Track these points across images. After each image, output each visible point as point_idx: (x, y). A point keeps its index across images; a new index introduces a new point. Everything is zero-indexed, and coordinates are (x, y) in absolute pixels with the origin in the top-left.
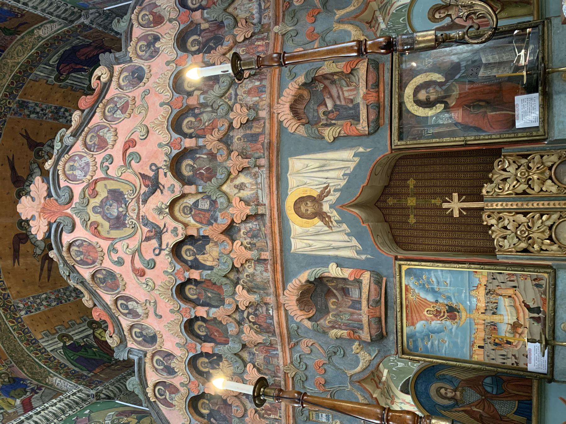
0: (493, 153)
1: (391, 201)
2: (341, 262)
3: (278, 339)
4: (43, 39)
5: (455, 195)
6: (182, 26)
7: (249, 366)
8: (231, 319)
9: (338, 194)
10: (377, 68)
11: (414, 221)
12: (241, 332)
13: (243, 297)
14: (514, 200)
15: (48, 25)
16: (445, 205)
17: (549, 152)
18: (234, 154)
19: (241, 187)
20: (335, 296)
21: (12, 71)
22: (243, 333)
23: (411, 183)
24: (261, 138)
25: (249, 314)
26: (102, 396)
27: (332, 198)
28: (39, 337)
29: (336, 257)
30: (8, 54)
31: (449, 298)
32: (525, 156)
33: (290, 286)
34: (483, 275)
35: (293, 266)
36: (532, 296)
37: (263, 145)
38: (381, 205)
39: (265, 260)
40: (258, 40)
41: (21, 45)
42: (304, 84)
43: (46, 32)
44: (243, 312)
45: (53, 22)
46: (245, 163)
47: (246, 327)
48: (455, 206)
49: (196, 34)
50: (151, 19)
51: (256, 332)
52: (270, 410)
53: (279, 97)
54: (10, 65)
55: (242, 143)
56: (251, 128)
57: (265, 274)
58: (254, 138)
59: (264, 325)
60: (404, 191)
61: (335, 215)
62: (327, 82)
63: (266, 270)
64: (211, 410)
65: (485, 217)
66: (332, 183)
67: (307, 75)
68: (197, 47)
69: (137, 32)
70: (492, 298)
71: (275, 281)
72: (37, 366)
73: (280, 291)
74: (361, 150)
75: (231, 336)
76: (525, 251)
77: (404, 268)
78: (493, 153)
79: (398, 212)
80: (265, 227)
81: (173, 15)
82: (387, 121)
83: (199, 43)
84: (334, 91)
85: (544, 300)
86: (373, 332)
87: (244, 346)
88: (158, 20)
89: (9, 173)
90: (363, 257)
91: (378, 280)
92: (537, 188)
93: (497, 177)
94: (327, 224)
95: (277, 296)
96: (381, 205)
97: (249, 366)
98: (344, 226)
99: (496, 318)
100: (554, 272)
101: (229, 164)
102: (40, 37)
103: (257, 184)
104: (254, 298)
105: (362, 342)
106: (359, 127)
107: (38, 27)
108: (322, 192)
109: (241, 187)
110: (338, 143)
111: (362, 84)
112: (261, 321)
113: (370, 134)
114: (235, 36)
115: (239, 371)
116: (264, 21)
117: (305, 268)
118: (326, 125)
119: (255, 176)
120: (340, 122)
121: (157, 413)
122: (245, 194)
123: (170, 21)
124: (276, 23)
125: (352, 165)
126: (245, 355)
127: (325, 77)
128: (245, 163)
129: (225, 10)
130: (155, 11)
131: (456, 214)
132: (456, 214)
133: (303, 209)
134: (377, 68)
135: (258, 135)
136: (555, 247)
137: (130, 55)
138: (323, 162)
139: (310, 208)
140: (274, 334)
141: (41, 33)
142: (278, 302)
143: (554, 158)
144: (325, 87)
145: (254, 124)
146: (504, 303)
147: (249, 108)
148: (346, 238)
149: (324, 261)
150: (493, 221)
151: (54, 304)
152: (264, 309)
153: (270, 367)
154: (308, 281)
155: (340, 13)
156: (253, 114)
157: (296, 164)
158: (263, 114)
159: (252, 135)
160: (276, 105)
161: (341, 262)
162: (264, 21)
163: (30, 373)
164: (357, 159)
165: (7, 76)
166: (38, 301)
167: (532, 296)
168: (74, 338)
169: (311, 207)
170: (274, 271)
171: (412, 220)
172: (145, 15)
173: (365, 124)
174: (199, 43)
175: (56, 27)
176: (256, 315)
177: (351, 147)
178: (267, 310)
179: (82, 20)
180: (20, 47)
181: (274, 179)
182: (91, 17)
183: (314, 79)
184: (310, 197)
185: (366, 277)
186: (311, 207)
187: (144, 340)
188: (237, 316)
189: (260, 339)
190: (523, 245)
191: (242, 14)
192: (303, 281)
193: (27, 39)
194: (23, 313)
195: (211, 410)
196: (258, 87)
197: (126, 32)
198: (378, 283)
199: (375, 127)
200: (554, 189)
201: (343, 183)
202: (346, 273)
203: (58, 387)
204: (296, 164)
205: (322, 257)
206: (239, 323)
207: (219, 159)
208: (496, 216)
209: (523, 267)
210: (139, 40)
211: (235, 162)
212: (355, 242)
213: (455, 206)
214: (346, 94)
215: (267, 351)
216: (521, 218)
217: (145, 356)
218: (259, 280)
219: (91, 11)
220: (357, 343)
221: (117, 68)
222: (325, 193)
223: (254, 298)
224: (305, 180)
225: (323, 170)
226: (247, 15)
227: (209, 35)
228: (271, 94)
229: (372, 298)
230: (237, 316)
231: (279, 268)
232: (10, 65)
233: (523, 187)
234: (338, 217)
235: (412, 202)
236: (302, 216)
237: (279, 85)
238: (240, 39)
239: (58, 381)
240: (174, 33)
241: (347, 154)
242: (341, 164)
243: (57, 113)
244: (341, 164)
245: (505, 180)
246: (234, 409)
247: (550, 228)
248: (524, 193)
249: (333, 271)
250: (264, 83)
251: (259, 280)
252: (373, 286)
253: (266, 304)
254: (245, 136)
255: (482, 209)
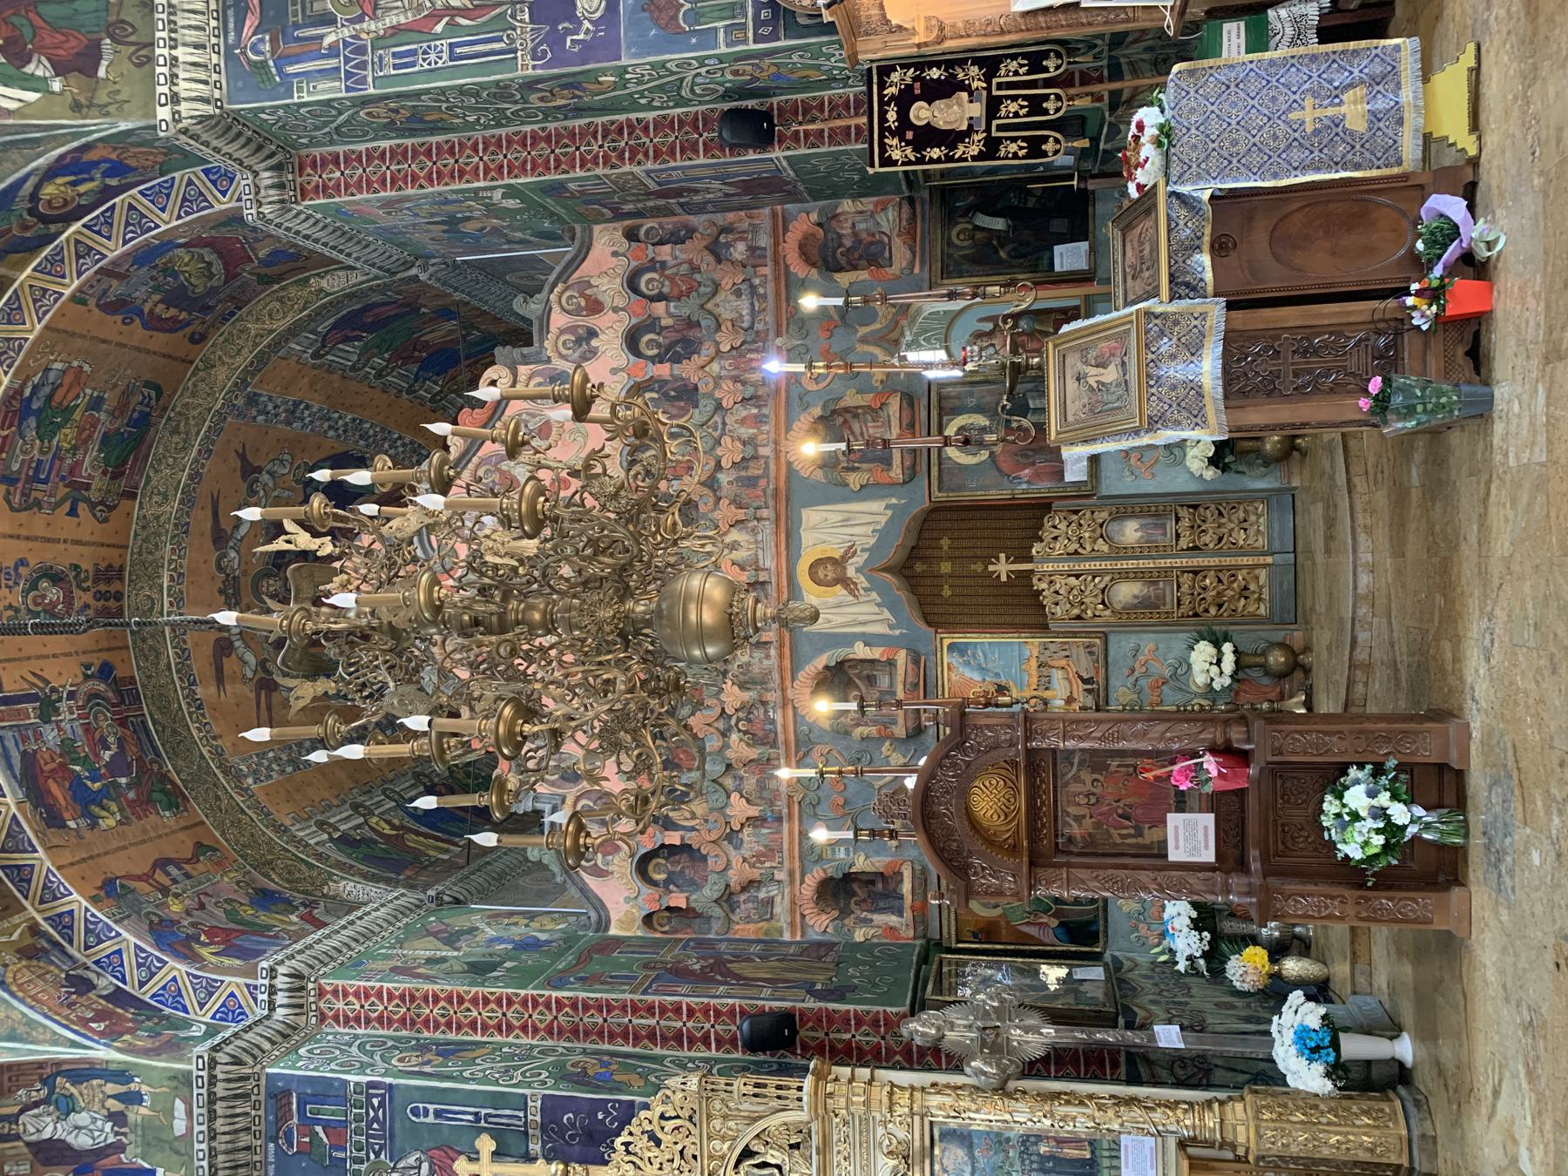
0: (1043, 507)
1: (919, 567)
2: (869, 641)
3: (782, 751)
4: (328, 294)
5: (1002, 556)
6: (634, 321)
7: (735, 797)
8: (712, 730)
9: (866, 555)
10: (912, 405)
11: (949, 593)
12: (726, 746)
13: (733, 696)
14: (1066, 561)
15: (341, 273)
16: (991, 568)
17: (1101, 508)
18: (724, 503)
19: (734, 546)
20: (858, 688)
21: (256, 345)
22: (729, 747)
23: (945, 542)
24: (763, 483)
25: (739, 720)
26: (446, 898)
27: (859, 560)
28: (288, 822)
29: (864, 634)
30: (250, 313)
31: (997, 675)
32: (1076, 512)
33: (801, 675)
34: (1032, 645)
35: (805, 649)
36: (1085, 666)
37: (764, 491)
38: (907, 573)
39: (766, 643)
40: (751, 351)
41: (280, 300)
42: (821, 418)
43: (334, 283)
44: (730, 717)
45: (354, 268)
46: (741, 514)
47: (735, 737)
48: (1003, 568)
49: (654, 332)
50: (583, 303)
51: (748, 745)
52: (763, 855)
53: (787, 432)
54: (253, 333)
55: (734, 487)
56: (747, 468)
57: (766, 662)
58: (751, 482)
59: (760, 733)
60: (936, 553)
61: (862, 582)
62: (848, 416)
63: (768, 657)
64: (670, 874)
65: (1035, 581)
66: (859, 541)
67: (824, 407)
68: (655, 352)
69: (558, 320)
70: (1045, 671)
71: (781, 669)
72: (303, 867)
73: (788, 683)
74: (894, 501)
75: (710, 754)
76: (1079, 617)
77: (946, 642)
78: (1043, 507)
79: (928, 582)
80: (345, 842)
81: (620, 302)
82: (925, 468)
83: (659, 345)
84: (856, 427)
85: (1097, 669)
86: (910, 724)
87: (729, 766)
88: (595, 307)
89: (209, 524)
90: (897, 632)
91: (915, 659)
92: (1089, 548)
93: (1047, 535)
94: (851, 592)
95: (783, 690)
96: (907, 573)
97: (735, 797)
98: (874, 595)
99: (1047, 694)
100: (1105, 637)
101: (717, 515)
102: (321, 290)
103: (756, 542)
104: (747, 696)
105: (894, 739)
106: (892, 474)
107: (318, 275)
108: (846, 553)
109: (734, 546)
110: (865, 493)
111: (895, 423)
112: (756, 729)
113: (905, 483)
114: (717, 344)
115: (719, 805)
116: (759, 326)
117: (821, 651)
118: (848, 469)
119: (754, 531)
120: (865, 466)
121: (581, 890)
122: (739, 555)
123: (615, 310)
124: (778, 334)
125: (883, 520)
126: (729, 782)
127: (846, 410)
128: (741, 514)
129: (702, 306)
130: (588, 292)
131: (1004, 578)
132: (1004, 578)
133: (821, 573)
134: (912, 405)
135: (758, 477)
136: (1107, 613)
137: (549, 353)
138: (846, 515)
139: (830, 572)
140: (774, 745)
141: (324, 283)
142: (784, 697)
143: (1105, 515)
144: (846, 421)
145: (751, 464)
146: (1057, 675)
147: (744, 443)
148: (876, 609)
149: (849, 639)
150: (1044, 586)
151: (289, 769)
152: (762, 710)
153: (766, 794)
154: (827, 667)
155: (863, 331)
156: (749, 451)
157: (811, 517)
158: (765, 451)
159: (749, 478)
160: (783, 442)
161: (869, 641)
162: (759, 326)
163: (288, 881)
164: (889, 513)
165: (245, 351)
166: (266, 763)
167: (1085, 666)
168: (343, 827)
169: (831, 571)
170: (781, 656)
171: (947, 592)
172: (572, 297)
173: (899, 471)
174: (659, 345)
175: (356, 278)
176: (749, 721)
177: (882, 497)
178: (766, 711)
179: (414, 271)
180: (277, 305)
181: (783, 536)
182: (432, 269)
183: (834, 412)
184: (830, 559)
185: (901, 657)
186: (831, 571)
187: (562, 778)
188: (721, 725)
189: (753, 753)
190: (1076, 611)
191: (726, 314)
192: (820, 667)
193: (293, 292)
194: (250, 780)
195: (670, 874)
196: (756, 416)
197: (541, 319)
198: (916, 662)
199: (911, 474)
200: (1105, 548)
201: (872, 541)
202: (876, 653)
203: (351, 898)
204: (811, 517)
205: (845, 635)
206: (724, 734)
207: (702, 508)
208: (1047, 579)
209: (1074, 635)
210: (562, 332)
211: (726, 512)
212: (887, 614)
213: (1003, 568)
214: (871, 431)
215: (761, 772)
216: (1072, 581)
217: (563, 802)
218: (756, 670)
219: (433, 261)
220: (887, 743)
221: (523, 370)
222: (850, 553)
223: (747, 696)
224: (824, 537)
225: (846, 527)
226: (734, 315)
227: (674, 336)
228: (777, 427)
229: (909, 680)
230: (721, 725)
231: (787, 652)
232: (253, 333)
233: (1074, 546)
234: (866, 584)
235: (946, 568)
236: (819, 583)
237: (787, 415)
238: (725, 348)
239: (350, 887)
240: (621, 328)
241: (876, 506)
242: (870, 518)
243: (293, 412)
244: (870, 518)
245: (1055, 538)
246: (710, 861)
247: (1103, 591)
248: (1076, 553)
249: (861, 651)
250: (765, 411)
251: (756, 670)
252: (910, 666)
253: (764, 703)
254: (738, 479)
255: (1032, 571)
